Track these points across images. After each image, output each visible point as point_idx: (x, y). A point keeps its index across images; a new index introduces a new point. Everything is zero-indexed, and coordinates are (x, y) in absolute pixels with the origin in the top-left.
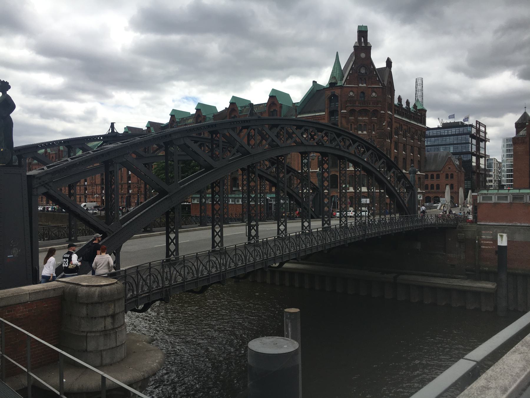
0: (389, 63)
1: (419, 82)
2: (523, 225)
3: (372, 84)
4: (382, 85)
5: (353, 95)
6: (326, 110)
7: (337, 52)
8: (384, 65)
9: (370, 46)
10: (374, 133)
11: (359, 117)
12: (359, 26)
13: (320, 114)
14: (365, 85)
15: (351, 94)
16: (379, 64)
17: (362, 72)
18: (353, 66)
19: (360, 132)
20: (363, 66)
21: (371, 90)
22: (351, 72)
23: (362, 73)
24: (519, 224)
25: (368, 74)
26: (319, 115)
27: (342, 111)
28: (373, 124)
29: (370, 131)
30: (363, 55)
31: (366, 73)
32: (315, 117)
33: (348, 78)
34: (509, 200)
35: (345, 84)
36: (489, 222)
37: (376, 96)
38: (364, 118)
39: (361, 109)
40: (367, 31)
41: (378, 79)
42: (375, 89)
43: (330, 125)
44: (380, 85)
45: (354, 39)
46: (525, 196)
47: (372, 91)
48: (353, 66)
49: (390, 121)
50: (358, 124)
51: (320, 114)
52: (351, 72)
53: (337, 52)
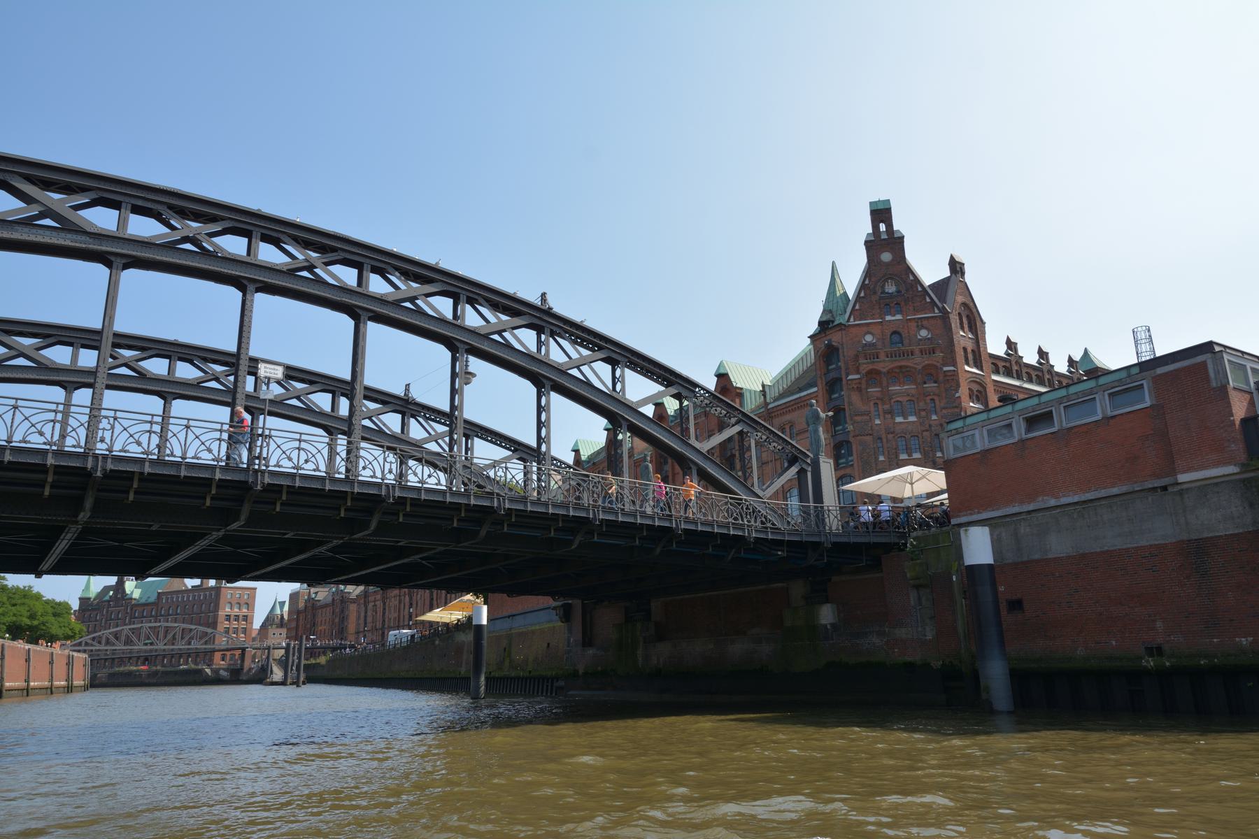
0: (956, 267)
1: (1142, 335)
2: (1064, 500)
3: (916, 311)
4: (940, 312)
5: (874, 341)
6: (819, 382)
7: (833, 263)
8: (946, 273)
9: (899, 235)
10: (934, 417)
11: (894, 385)
12: (871, 203)
13: (809, 392)
14: (899, 317)
15: (869, 338)
16: (930, 270)
17: (890, 291)
18: (867, 282)
19: (899, 419)
20: (891, 278)
21: (916, 324)
22: (862, 295)
23: (888, 293)
24: (1053, 502)
25: (903, 292)
26: (808, 395)
27: (850, 377)
28: (931, 397)
29: (923, 414)
30: (886, 257)
31: (899, 292)
32: (799, 400)
33: (857, 307)
34: (1016, 434)
35: (852, 319)
36: (979, 513)
37: (929, 336)
38: (905, 387)
39: (892, 366)
40: (890, 208)
41: (928, 300)
42: (925, 323)
43: (808, 402)
44: (936, 311)
45: (865, 227)
46: (1053, 409)
47: (918, 326)
48: (867, 282)
49: (980, 389)
50: (892, 401)
51: (809, 392)
52: (862, 295)
53: (833, 263)
